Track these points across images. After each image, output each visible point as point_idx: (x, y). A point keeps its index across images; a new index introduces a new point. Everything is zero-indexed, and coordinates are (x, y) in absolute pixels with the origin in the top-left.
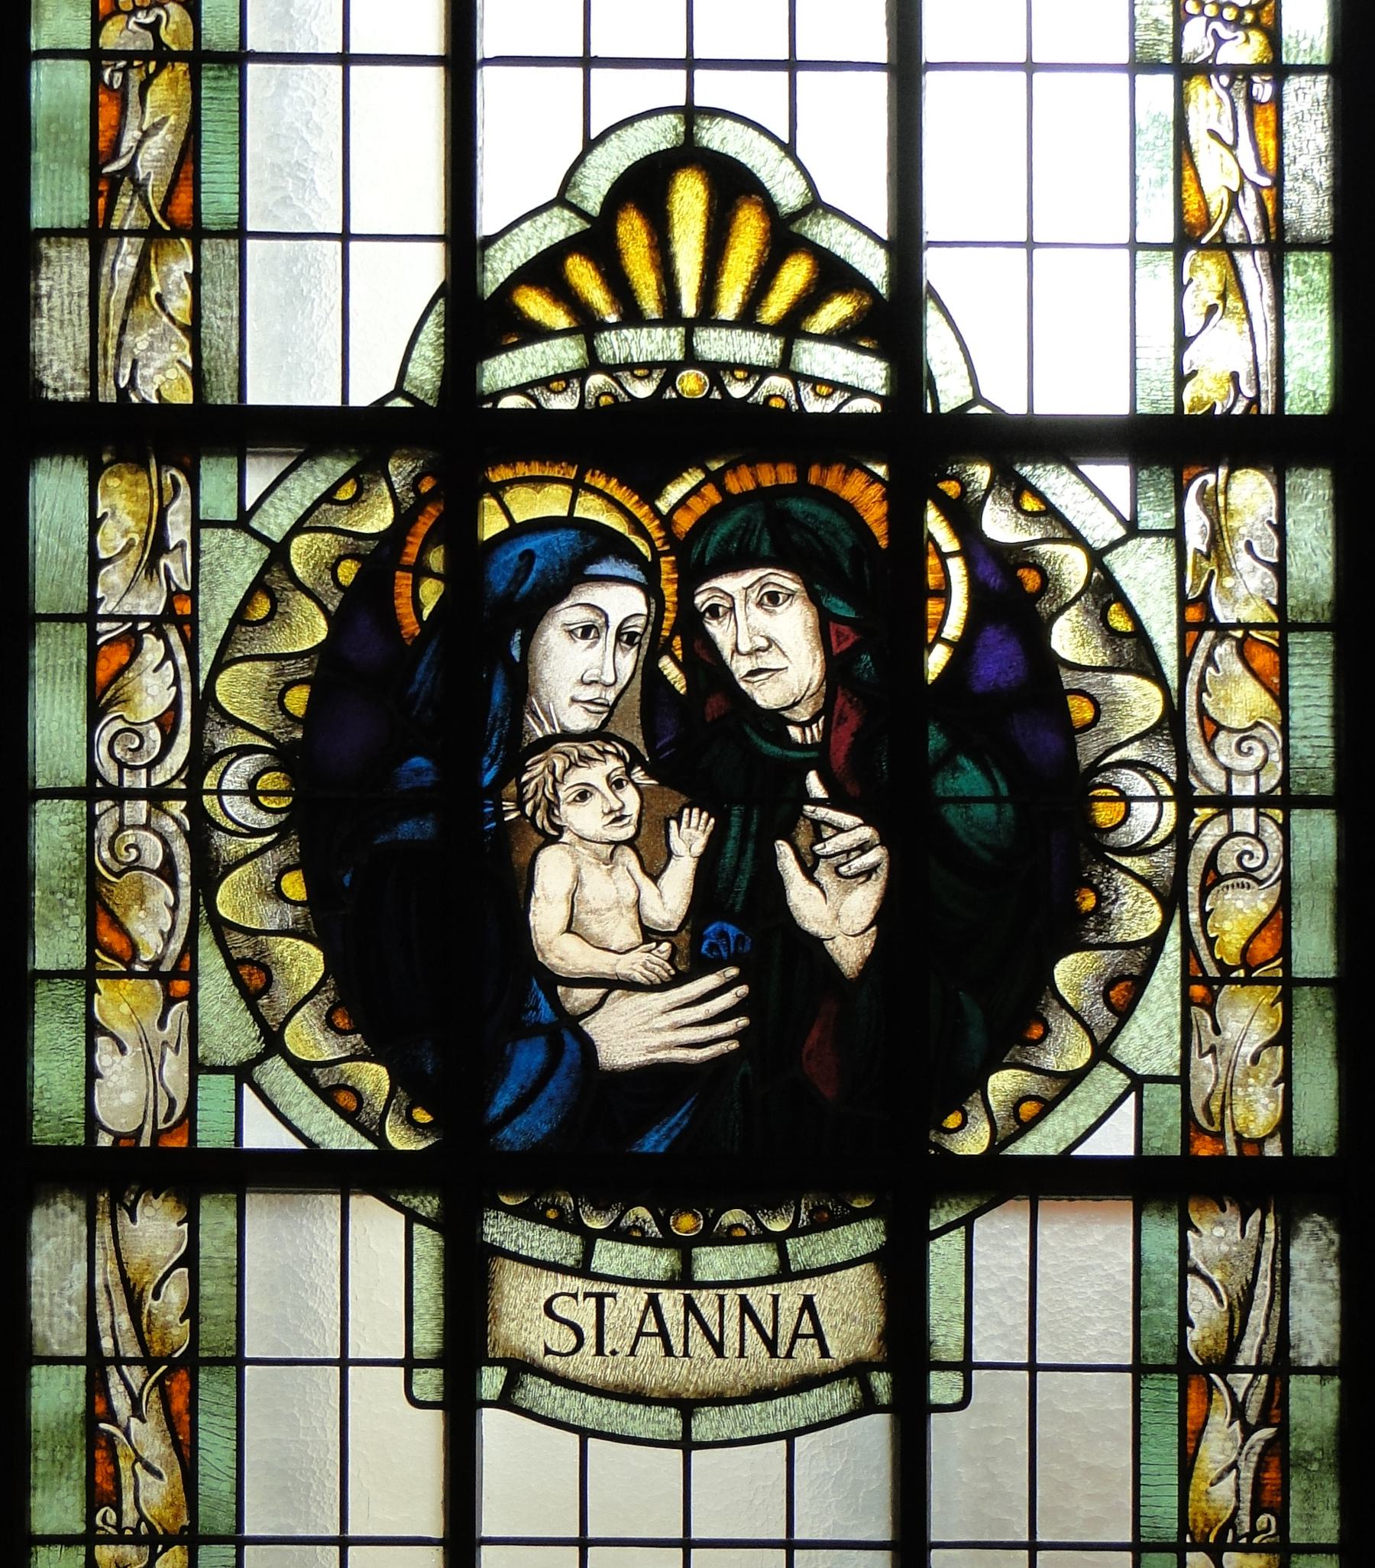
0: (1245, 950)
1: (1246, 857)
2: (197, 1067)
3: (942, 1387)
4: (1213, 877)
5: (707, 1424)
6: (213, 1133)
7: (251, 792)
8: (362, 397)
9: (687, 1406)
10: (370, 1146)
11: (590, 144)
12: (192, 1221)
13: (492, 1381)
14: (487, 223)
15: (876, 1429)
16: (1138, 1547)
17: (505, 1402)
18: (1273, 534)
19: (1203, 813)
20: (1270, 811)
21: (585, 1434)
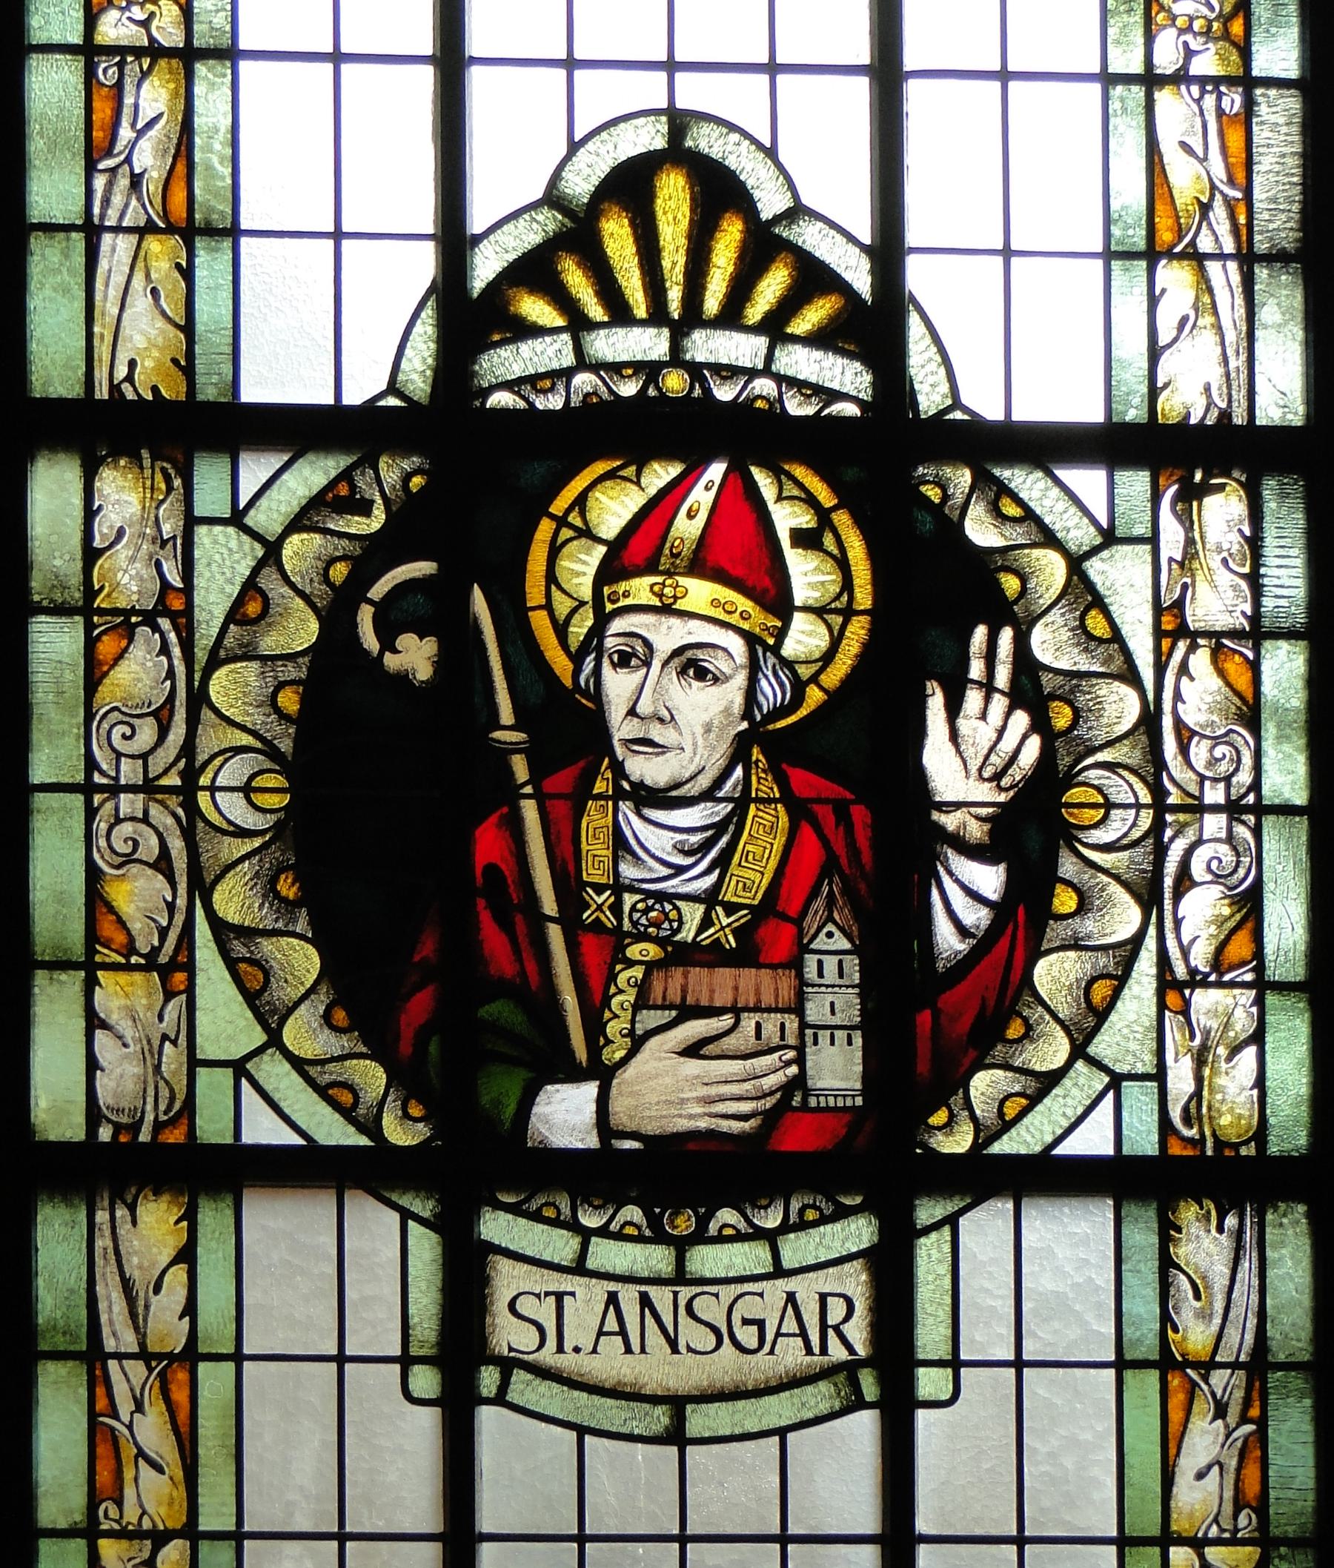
0: (131, 640)
1: (129, 733)
2: (194, 1063)
3: (930, 1382)
4: (163, 717)
5: (700, 1420)
6: (1135, 483)
7: (247, 790)
8: (353, 397)
9: (678, 1403)
10: (363, 1141)
11: (574, 147)
12: (190, 1216)
13: (489, 1379)
14: (477, 221)
15: (865, 1425)
16: (1123, 1542)
17: (500, 1399)
18: (101, 1060)
19: (173, 780)
20: (105, 781)
21: (582, 1431)
